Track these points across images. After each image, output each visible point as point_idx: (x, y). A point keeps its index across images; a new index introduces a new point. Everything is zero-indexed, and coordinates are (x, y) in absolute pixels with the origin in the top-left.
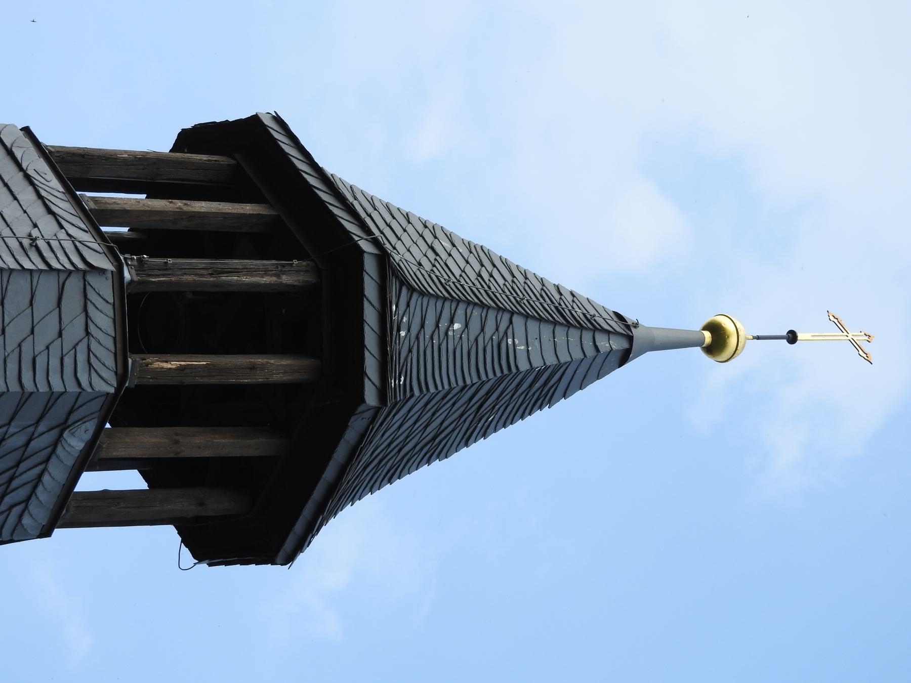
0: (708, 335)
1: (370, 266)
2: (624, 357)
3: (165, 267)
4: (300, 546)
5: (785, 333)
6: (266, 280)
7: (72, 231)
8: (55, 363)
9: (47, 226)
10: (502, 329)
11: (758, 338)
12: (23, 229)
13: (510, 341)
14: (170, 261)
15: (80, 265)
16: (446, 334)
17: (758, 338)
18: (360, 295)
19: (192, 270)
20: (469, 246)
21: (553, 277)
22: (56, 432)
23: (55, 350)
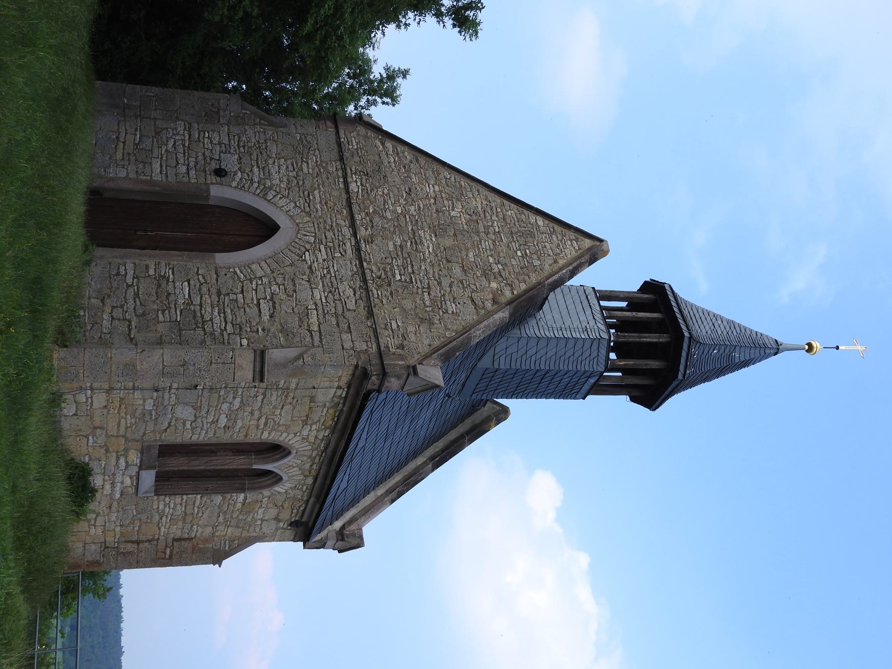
0: (807, 347)
1: (686, 340)
2: (776, 354)
3: (625, 336)
4: (657, 407)
5: (835, 347)
6: (655, 340)
7: (599, 325)
8: (587, 363)
9: (592, 323)
10: (732, 350)
11: (825, 348)
12: (584, 324)
13: (733, 354)
14: (626, 334)
15: (599, 337)
16: (711, 354)
17: (825, 348)
18: (682, 348)
19: (633, 337)
20: (728, 321)
21: (755, 328)
22: (587, 378)
23: (588, 359)
